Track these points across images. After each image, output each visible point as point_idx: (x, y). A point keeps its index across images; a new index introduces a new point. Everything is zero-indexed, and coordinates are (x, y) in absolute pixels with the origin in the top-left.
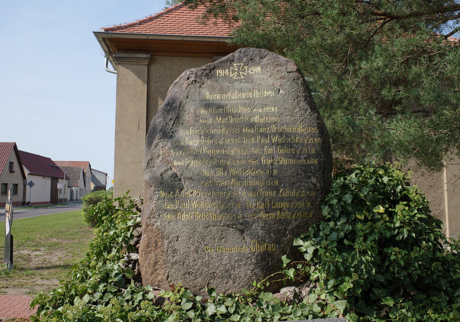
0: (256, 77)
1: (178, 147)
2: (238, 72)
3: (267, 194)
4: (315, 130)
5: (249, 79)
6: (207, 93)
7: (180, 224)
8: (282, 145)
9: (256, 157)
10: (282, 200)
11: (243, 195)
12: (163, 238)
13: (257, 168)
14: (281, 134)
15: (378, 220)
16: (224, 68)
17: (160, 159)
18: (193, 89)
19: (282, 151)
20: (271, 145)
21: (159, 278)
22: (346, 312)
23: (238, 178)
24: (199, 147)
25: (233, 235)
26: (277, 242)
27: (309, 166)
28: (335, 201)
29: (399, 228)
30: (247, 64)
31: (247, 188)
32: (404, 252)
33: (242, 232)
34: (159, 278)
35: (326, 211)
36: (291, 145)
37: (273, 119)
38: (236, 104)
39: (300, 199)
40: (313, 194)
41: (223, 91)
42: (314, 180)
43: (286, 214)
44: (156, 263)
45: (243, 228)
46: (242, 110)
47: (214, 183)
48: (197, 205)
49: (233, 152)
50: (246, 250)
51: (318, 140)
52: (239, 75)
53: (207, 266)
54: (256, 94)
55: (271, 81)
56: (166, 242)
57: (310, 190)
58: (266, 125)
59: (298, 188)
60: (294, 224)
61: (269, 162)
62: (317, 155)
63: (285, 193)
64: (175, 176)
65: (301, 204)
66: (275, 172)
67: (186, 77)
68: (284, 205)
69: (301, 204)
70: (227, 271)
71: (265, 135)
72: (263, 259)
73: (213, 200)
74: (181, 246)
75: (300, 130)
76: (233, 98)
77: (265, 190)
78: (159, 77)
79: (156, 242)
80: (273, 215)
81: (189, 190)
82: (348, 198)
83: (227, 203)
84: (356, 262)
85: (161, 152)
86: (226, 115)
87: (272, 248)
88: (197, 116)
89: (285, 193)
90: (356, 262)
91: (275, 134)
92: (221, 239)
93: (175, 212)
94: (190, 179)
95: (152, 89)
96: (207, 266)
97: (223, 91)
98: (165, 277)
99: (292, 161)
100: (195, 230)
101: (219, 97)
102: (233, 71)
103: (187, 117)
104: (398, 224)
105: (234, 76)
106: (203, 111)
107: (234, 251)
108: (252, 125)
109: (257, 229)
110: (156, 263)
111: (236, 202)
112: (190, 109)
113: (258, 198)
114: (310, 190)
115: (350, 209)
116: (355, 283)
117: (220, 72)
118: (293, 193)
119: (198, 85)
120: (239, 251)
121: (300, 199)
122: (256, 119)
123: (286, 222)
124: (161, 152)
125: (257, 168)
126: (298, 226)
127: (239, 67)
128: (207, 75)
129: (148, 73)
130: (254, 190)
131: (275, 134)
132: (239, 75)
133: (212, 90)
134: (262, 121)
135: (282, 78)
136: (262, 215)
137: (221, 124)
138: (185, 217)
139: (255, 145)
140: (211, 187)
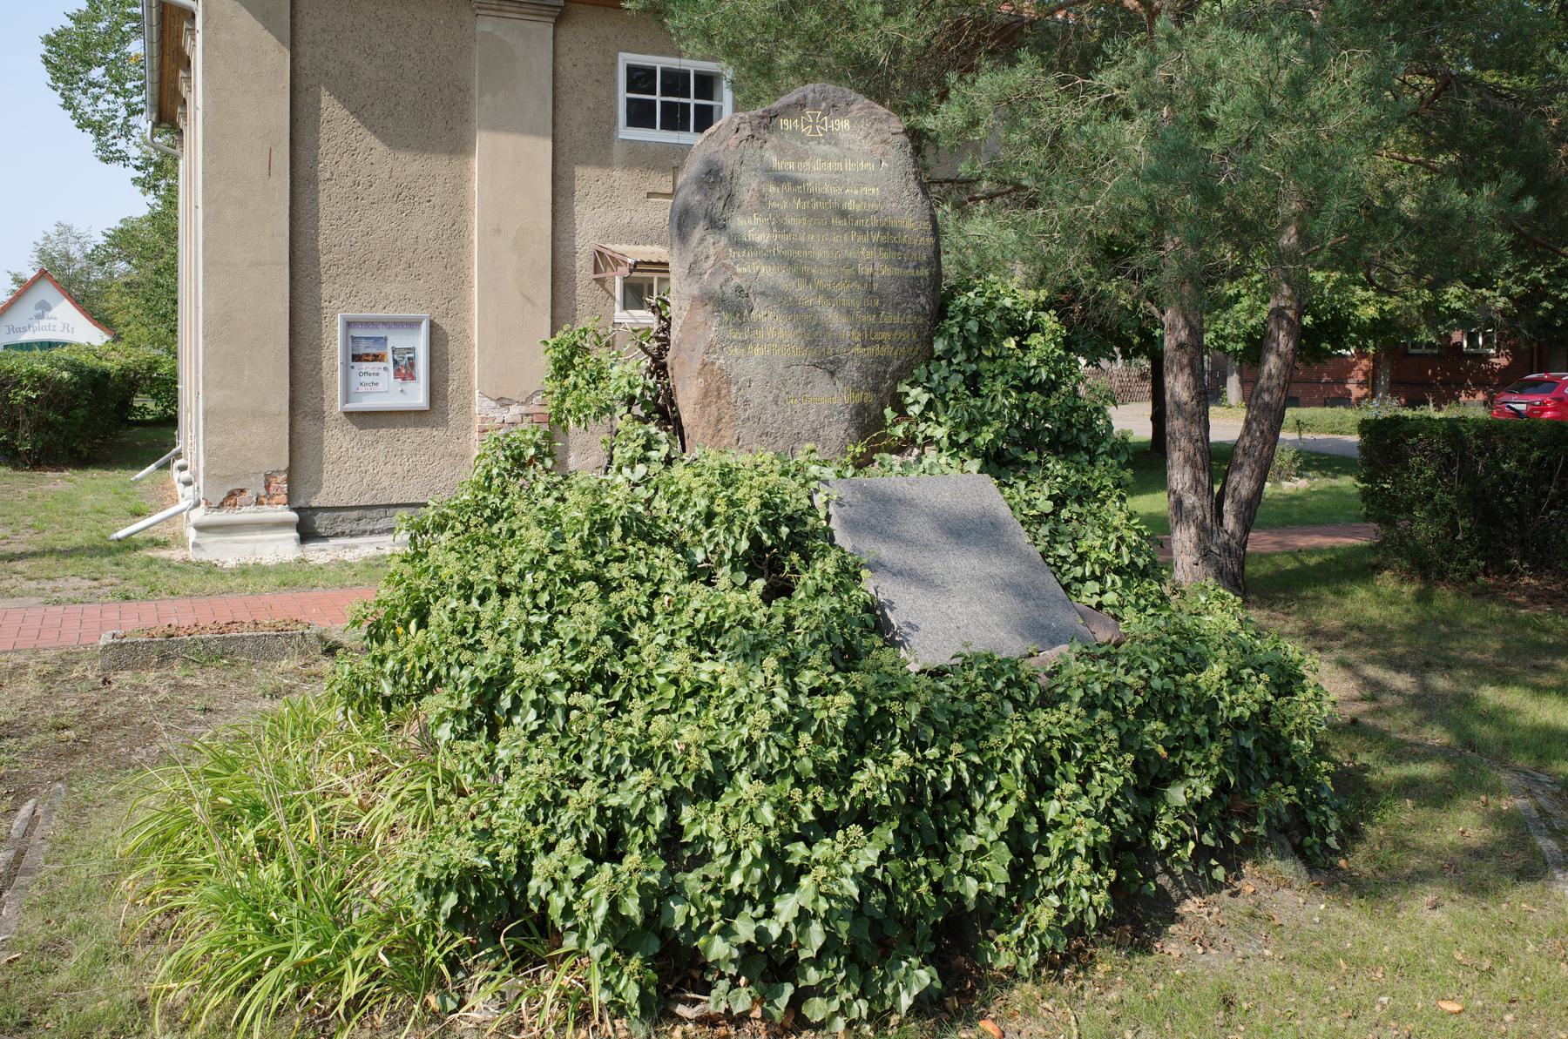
0: (842, 136)
1: (738, 243)
2: (814, 124)
3: (864, 318)
4: (927, 226)
5: (832, 139)
6: (775, 159)
7: (752, 362)
8: (886, 246)
9: (851, 264)
10: (882, 328)
11: (834, 319)
12: (729, 382)
13: (852, 279)
14: (884, 230)
15: (1010, 357)
16: (790, 117)
17: (711, 261)
18: (750, 150)
19: (885, 256)
20: (870, 245)
21: (725, 441)
22: (980, 472)
23: (829, 296)
24: (770, 246)
25: (821, 377)
26: (875, 390)
27: (918, 279)
28: (956, 330)
29: (1035, 367)
30: (826, 113)
31: (839, 308)
32: (1042, 398)
33: (832, 374)
34: (725, 441)
35: (940, 345)
36: (896, 247)
37: (874, 206)
38: (822, 180)
39: (904, 327)
40: (921, 321)
41: (799, 157)
42: (922, 300)
43: (887, 350)
44: (719, 420)
45: (832, 369)
46: (829, 189)
47: (795, 302)
48: (774, 334)
49: (819, 255)
50: (837, 401)
51: (930, 240)
52: (814, 131)
53: (790, 423)
54: (849, 166)
55: (867, 146)
56: (734, 389)
57: (917, 314)
58: (864, 215)
59: (903, 311)
60: (896, 364)
61: (869, 270)
62: (929, 263)
63: (889, 318)
64: (739, 289)
65: (905, 335)
66: (876, 286)
67: (734, 127)
68: (885, 335)
69: (905, 335)
70: (815, 431)
71: (861, 230)
72: (858, 414)
73: (795, 327)
74: (754, 394)
75: (909, 226)
76: (816, 170)
77: (863, 313)
78: (324, 31)
79: (719, 389)
80: (870, 349)
81: (761, 312)
82: (973, 325)
83: (813, 333)
84: (997, 407)
85: (712, 251)
86: (807, 196)
87: (869, 398)
88: (762, 198)
89: (889, 318)
90: (997, 407)
91: (876, 230)
92: (807, 384)
93: (745, 343)
94: (763, 293)
95: (304, 61)
96: (790, 423)
97: (799, 157)
98: (734, 441)
99: (898, 271)
100: (772, 370)
101: (792, 166)
102: (806, 124)
103: (746, 195)
104: (1034, 363)
105: (807, 131)
106: (772, 189)
107: (824, 402)
108: (844, 214)
109: (851, 370)
110: (719, 420)
111: (826, 330)
112: (748, 186)
113: (853, 324)
114: (917, 314)
115: (974, 341)
116: (996, 433)
117: (784, 122)
118: (897, 319)
119: (757, 144)
120: (832, 400)
121: (904, 327)
122: (850, 205)
123: (886, 361)
124: (712, 251)
125: (852, 279)
126: (900, 367)
127: (814, 116)
128: (766, 127)
129: (292, 17)
130: (849, 312)
131: (876, 230)
132: (814, 131)
133: (781, 152)
134: (858, 208)
135: (884, 142)
136: (857, 349)
137: (800, 210)
138: (758, 352)
139: (849, 245)
140: (791, 307)
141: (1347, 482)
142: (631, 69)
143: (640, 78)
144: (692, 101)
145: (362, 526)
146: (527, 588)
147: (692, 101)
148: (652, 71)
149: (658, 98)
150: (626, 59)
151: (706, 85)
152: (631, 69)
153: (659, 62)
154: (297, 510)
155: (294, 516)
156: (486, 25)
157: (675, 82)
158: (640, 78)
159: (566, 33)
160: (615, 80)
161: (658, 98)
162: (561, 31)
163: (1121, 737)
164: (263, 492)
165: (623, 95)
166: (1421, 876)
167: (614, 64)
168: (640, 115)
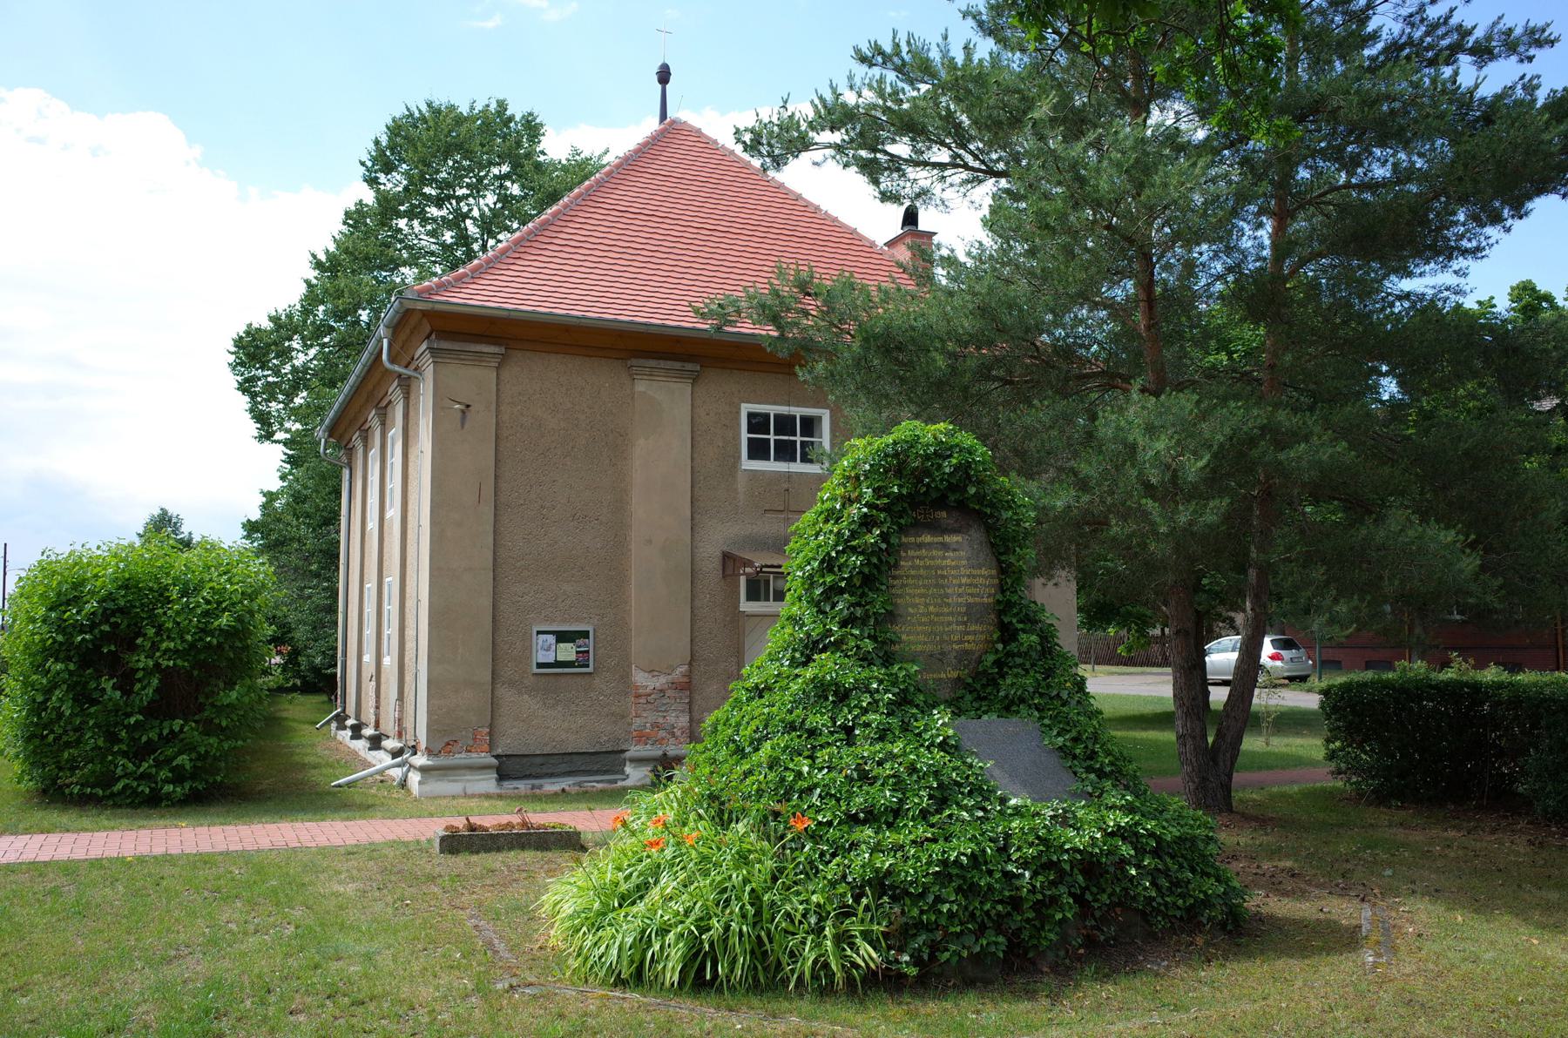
141: (1169, 736)
142: (751, 415)
143: (758, 423)
144: (798, 439)
145: (539, 760)
146: (790, 607)
147: (798, 439)
148: (767, 416)
149: (772, 437)
150: (746, 408)
151: (810, 425)
152: (751, 415)
153: (772, 410)
154: (497, 757)
155: (494, 761)
156: (641, 386)
157: (785, 424)
158: (758, 423)
159: (506, 374)
160: (739, 425)
161: (772, 437)
162: (505, 374)
163: (1009, 940)
164: (471, 742)
165: (745, 435)
166: (1004, 570)
167: (738, 413)
168: (758, 450)
